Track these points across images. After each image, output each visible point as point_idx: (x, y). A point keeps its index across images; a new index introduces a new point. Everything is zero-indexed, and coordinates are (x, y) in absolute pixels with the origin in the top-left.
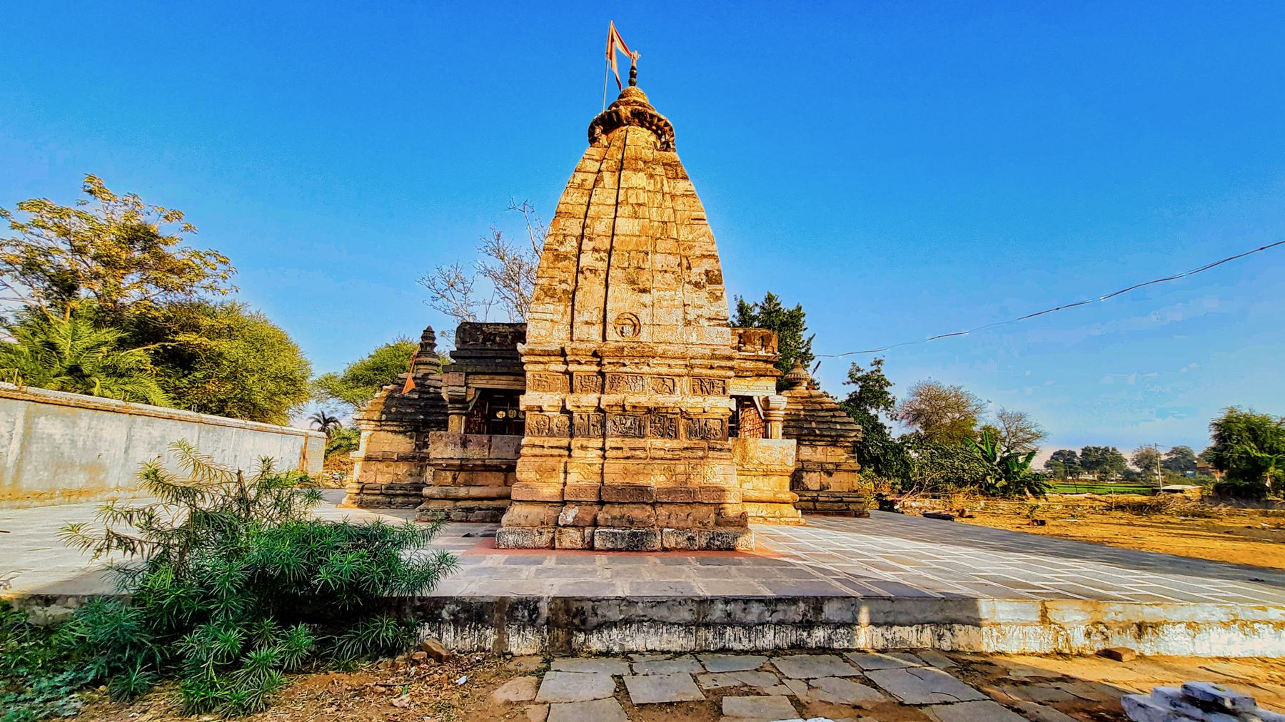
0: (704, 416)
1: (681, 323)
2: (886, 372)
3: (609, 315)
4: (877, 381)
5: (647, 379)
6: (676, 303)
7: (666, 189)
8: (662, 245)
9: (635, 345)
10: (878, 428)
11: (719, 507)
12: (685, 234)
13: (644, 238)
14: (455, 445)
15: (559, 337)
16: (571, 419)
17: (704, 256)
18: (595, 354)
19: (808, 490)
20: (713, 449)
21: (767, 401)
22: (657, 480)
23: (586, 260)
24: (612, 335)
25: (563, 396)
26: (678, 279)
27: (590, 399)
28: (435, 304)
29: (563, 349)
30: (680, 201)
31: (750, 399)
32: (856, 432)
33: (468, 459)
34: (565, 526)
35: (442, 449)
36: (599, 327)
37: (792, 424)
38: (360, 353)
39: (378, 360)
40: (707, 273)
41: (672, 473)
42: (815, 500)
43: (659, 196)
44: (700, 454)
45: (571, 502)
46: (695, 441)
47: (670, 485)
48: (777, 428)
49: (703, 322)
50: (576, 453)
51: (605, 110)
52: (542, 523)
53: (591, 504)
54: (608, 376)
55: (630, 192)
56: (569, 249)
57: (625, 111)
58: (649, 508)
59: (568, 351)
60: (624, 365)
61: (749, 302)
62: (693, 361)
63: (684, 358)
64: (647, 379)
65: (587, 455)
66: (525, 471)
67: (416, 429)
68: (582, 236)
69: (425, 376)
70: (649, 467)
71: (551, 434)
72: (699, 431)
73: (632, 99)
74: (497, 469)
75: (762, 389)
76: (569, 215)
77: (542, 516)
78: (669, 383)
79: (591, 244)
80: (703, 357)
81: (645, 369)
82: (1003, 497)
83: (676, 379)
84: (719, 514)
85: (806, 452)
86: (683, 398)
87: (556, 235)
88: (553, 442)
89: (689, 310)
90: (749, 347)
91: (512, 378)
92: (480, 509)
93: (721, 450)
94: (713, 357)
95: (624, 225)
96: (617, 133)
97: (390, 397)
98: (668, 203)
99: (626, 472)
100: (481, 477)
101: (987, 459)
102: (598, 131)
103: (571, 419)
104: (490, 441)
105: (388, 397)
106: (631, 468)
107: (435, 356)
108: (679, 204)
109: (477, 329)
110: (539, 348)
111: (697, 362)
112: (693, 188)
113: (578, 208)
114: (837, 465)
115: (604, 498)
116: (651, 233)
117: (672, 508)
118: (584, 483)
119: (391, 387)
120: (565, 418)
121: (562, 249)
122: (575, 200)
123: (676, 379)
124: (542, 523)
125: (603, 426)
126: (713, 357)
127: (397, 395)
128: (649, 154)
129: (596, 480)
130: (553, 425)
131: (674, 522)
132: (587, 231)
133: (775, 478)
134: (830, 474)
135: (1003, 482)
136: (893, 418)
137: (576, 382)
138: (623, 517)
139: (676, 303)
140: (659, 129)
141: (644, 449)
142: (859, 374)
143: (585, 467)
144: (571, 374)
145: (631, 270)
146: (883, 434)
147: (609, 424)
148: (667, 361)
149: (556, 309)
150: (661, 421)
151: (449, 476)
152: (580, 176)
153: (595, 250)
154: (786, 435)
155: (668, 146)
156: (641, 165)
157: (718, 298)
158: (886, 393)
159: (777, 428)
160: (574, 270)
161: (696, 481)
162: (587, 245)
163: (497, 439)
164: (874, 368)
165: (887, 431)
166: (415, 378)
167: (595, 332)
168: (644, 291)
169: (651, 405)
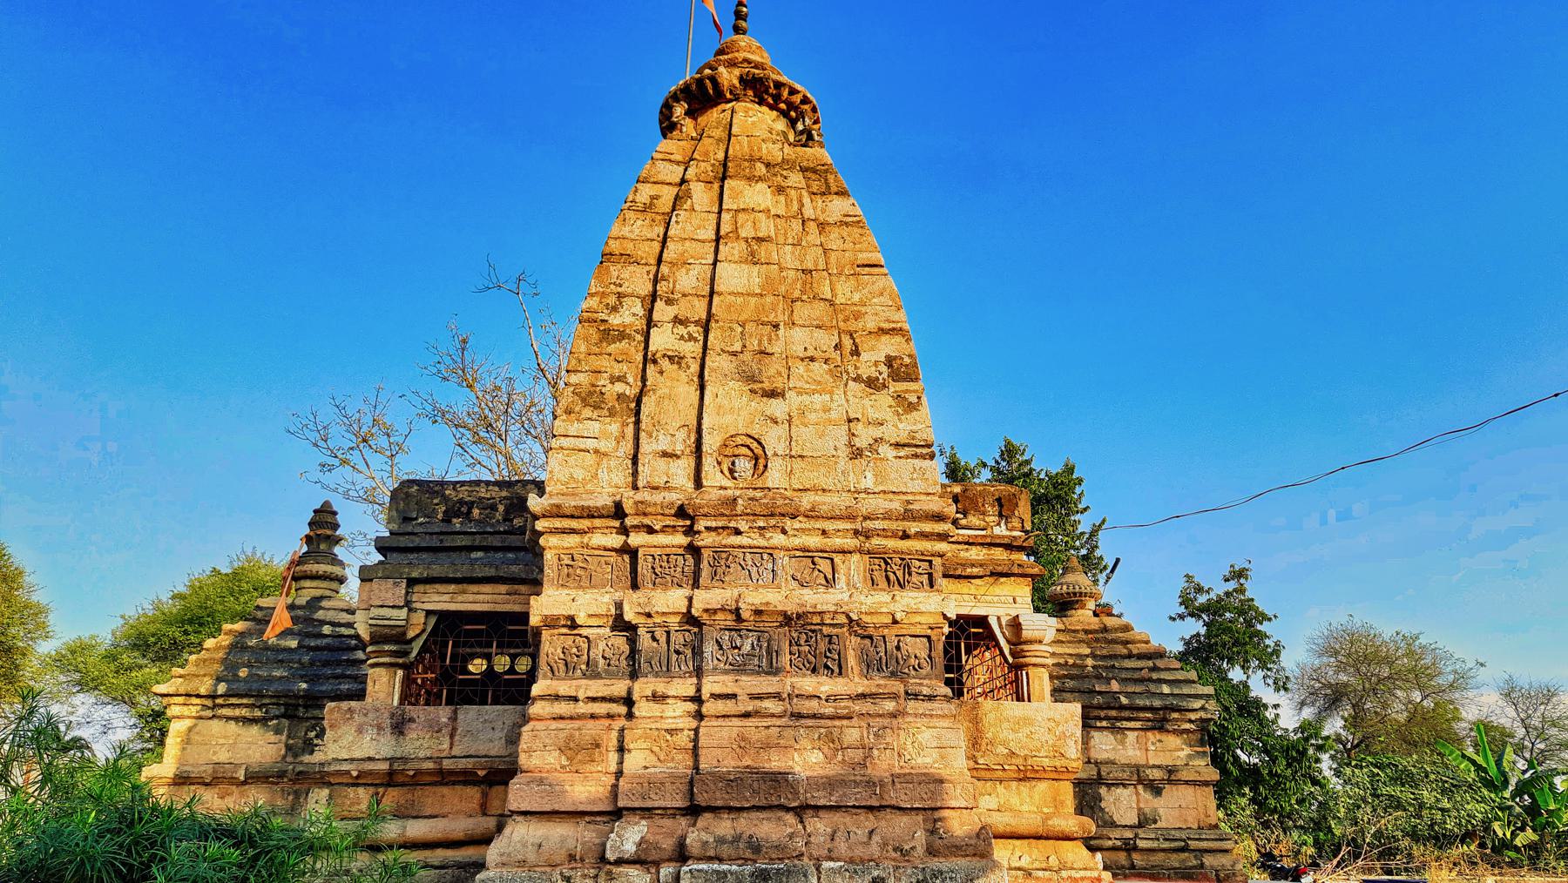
0: (895, 630)
1: (844, 452)
2: (1258, 593)
3: (706, 439)
4: (1241, 612)
5: (783, 560)
6: (833, 415)
7: (809, 212)
8: (803, 312)
9: (758, 494)
10: (1251, 708)
11: (931, 813)
12: (845, 292)
13: (769, 299)
14: (380, 728)
15: (609, 485)
16: (632, 641)
17: (882, 331)
18: (681, 512)
19: (1113, 825)
20: (916, 696)
21: (1015, 624)
22: (806, 761)
23: (662, 339)
24: (713, 477)
25: (618, 596)
26: (837, 373)
27: (671, 600)
28: (328, 478)
29: (618, 506)
30: (835, 233)
31: (982, 621)
32: (1204, 705)
33: (404, 759)
34: (620, 862)
35: (350, 739)
36: (687, 464)
37: (1070, 684)
38: (151, 588)
39: (194, 602)
40: (889, 361)
41: (833, 742)
42: (1129, 847)
43: (796, 225)
44: (890, 706)
45: (633, 809)
46: (879, 683)
47: (833, 770)
48: (1040, 682)
49: (886, 451)
50: (642, 709)
51: (688, 75)
52: (572, 858)
53: (667, 812)
54: (706, 553)
55: (741, 217)
56: (628, 319)
57: (728, 77)
58: (790, 818)
59: (628, 507)
60: (738, 532)
61: (967, 459)
62: (869, 524)
63: (851, 517)
64: (783, 560)
65: (665, 711)
66: (539, 752)
67: (290, 715)
68: (654, 296)
69: (315, 603)
70: (789, 733)
71: (592, 673)
72: (884, 660)
73: (741, 55)
74: (465, 778)
75: (1005, 602)
76: (627, 258)
77: (571, 844)
78: (824, 566)
79: (671, 311)
80: (887, 516)
81: (778, 539)
82: (1534, 866)
83: (838, 559)
84: (933, 832)
85: (1104, 745)
86: (852, 593)
87: (603, 295)
88: (597, 688)
89: (858, 428)
90: (973, 520)
91: (503, 588)
92: (426, 866)
93: (931, 698)
94: (909, 515)
95: (734, 276)
96: (714, 115)
97: (238, 646)
98: (813, 236)
99: (743, 743)
100: (430, 798)
101: (1490, 784)
102: (679, 110)
103: (632, 641)
104: (454, 718)
105: (232, 647)
106: (755, 736)
107: (335, 561)
108: (834, 239)
109: (435, 493)
110: (570, 503)
111: (878, 524)
112: (859, 212)
113: (646, 247)
114: (1171, 770)
115: (701, 799)
116: (783, 289)
117: (838, 818)
118: (658, 770)
119: (239, 626)
120: (620, 642)
121: (615, 320)
122: (637, 232)
123: (838, 559)
124: (572, 858)
125: (697, 652)
126: (909, 515)
127: (252, 642)
128: (774, 151)
129: (683, 765)
130: (596, 653)
131: (842, 847)
132: (662, 288)
133: (1042, 786)
134: (1156, 789)
135: (1529, 835)
136: (1281, 686)
137: (644, 567)
138: (737, 839)
139: (833, 415)
140: (791, 108)
141: (777, 696)
142: (1202, 599)
143: (659, 736)
144: (633, 553)
145: (747, 357)
146: (1262, 722)
147: (709, 648)
148: (819, 524)
149: (606, 432)
150: (812, 639)
151: (363, 795)
152: (645, 193)
153: (677, 321)
154: (1059, 694)
155: (810, 137)
156: (761, 169)
157: (912, 407)
158: (1259, 634)
159: (1040, 682)
160: (639, 357)
161: (883, 764)
162: (662, 311)
163: (470, 714)
164: (1232, 585)
165: (1270, 714)
166: (291, 607)
167: (681, 472)
168: (772, 394)
169: (791, 608)
